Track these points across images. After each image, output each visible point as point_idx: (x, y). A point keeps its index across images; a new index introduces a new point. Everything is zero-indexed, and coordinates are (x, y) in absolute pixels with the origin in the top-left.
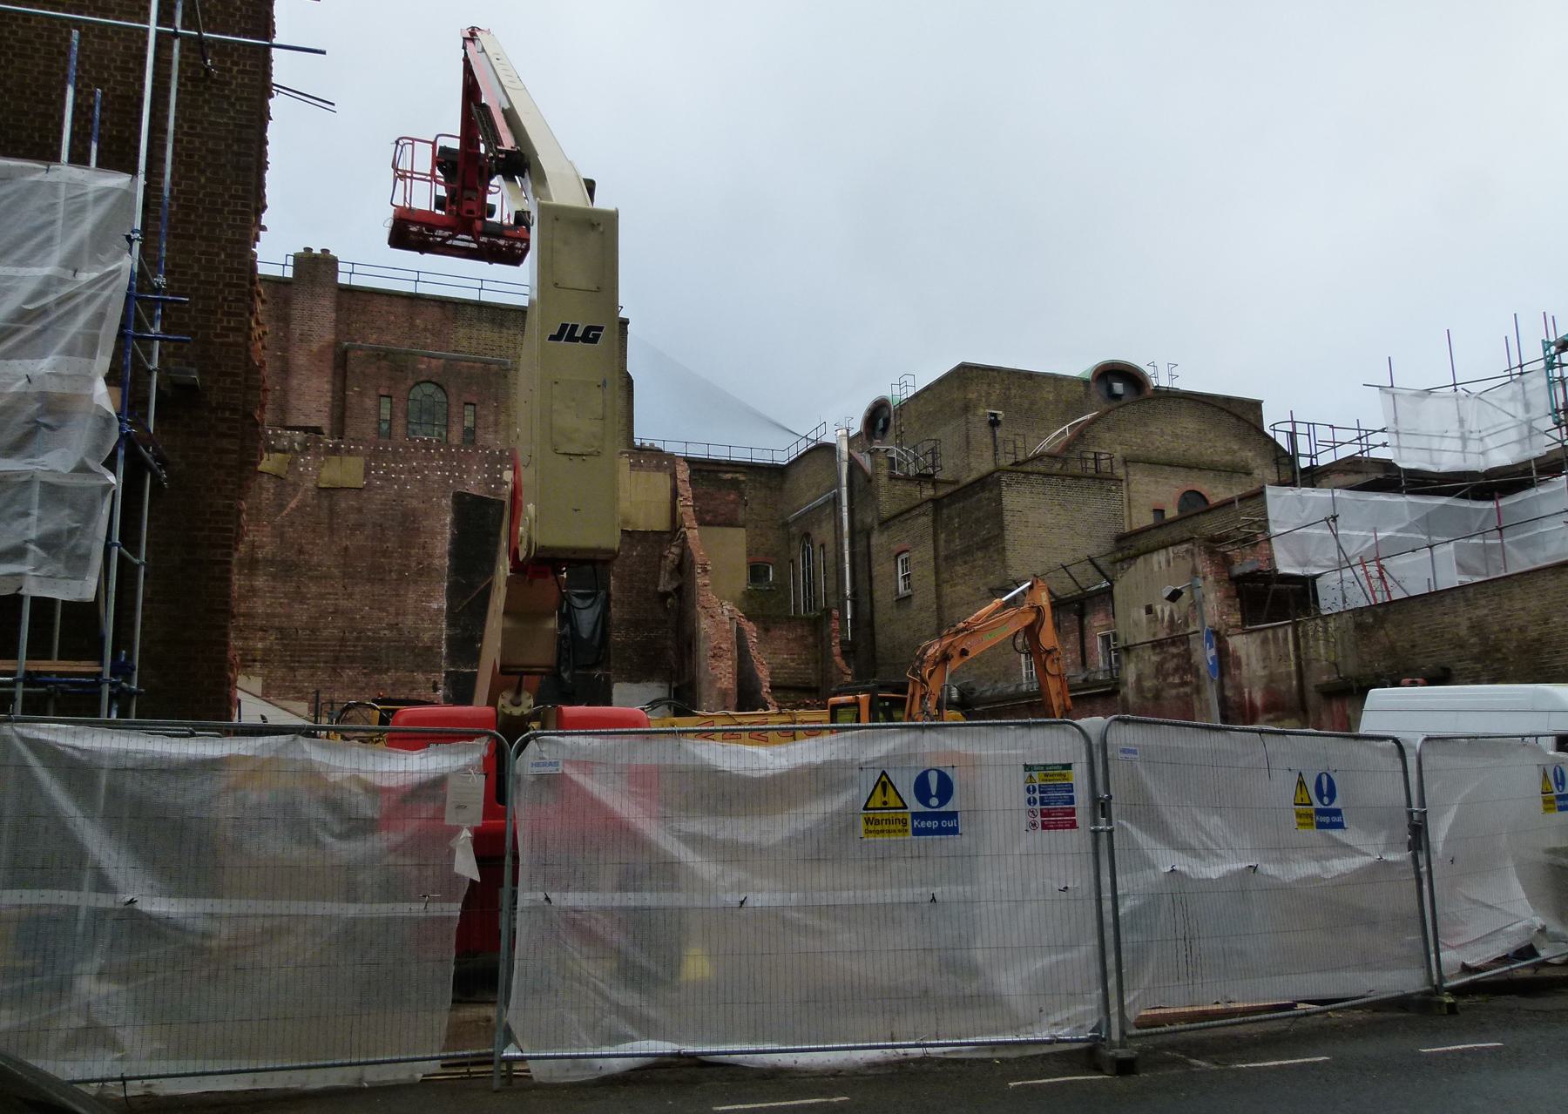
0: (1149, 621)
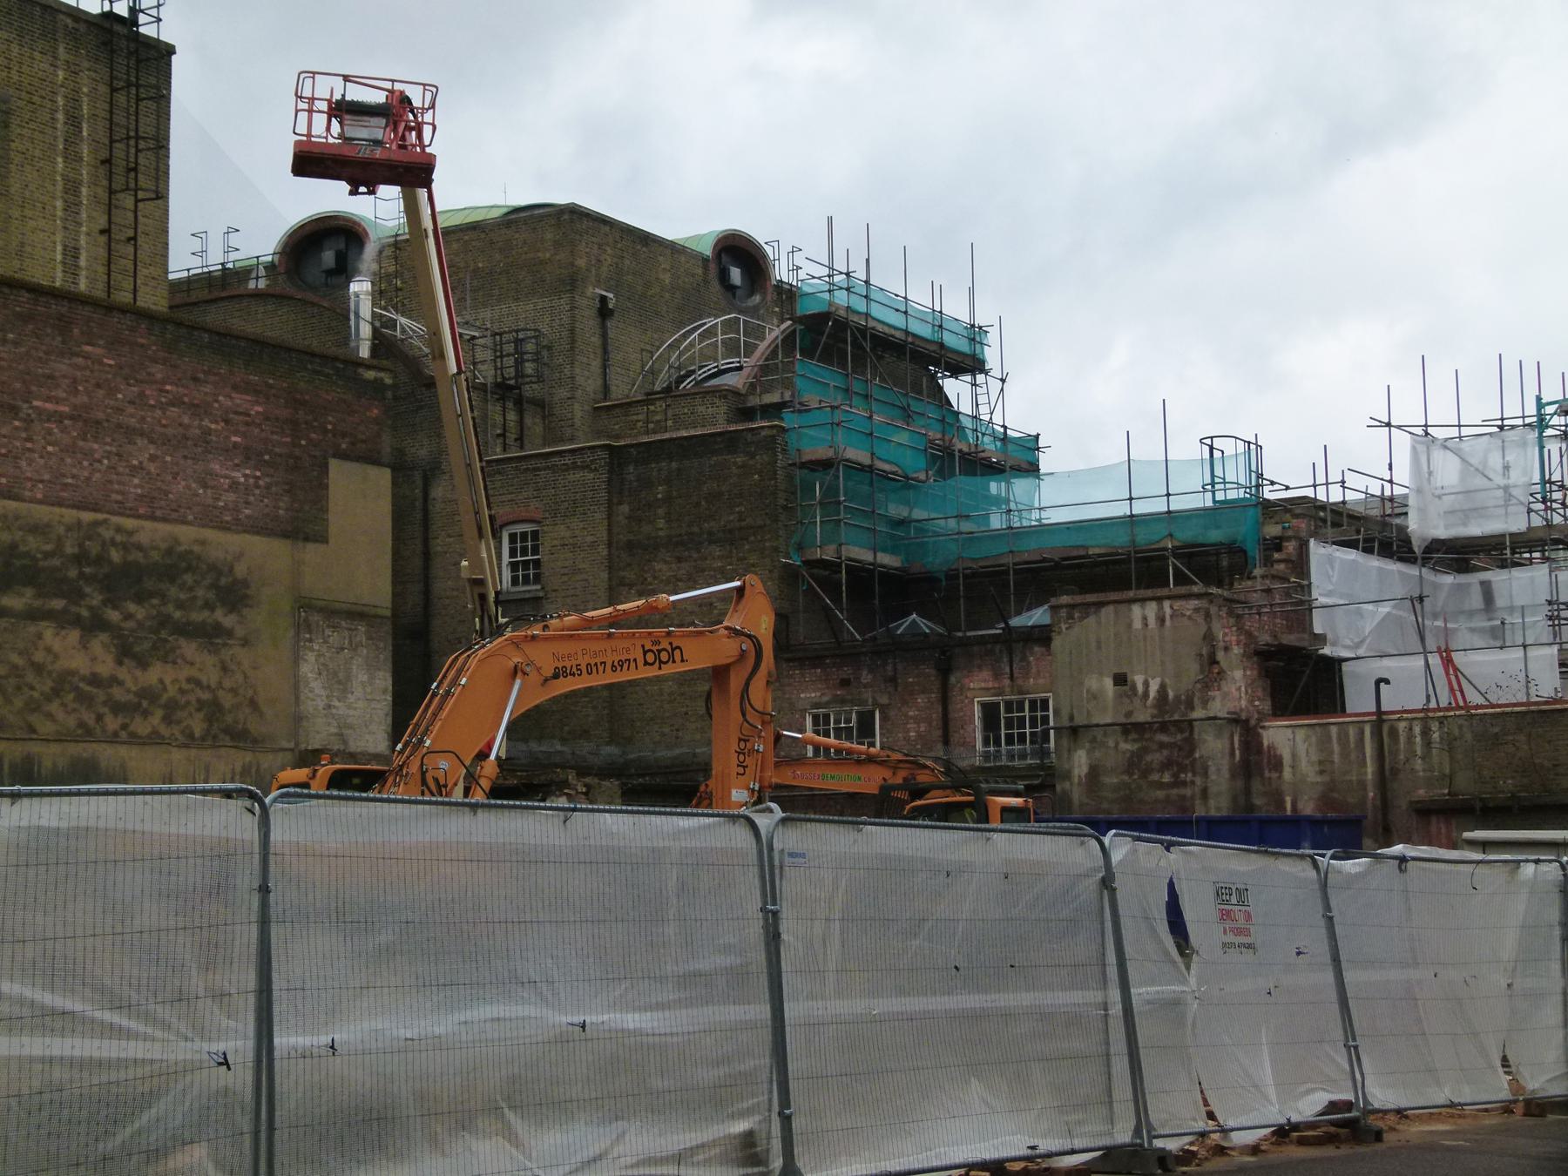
0: (1119, 697)
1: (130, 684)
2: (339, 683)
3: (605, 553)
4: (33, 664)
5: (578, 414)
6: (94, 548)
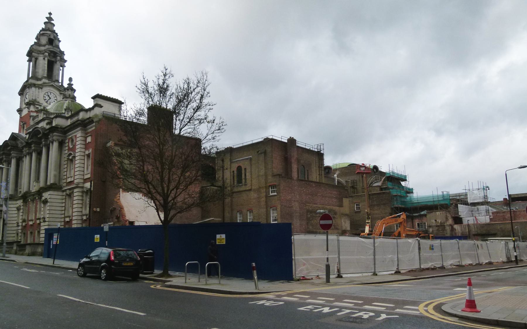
2: (345, 222)
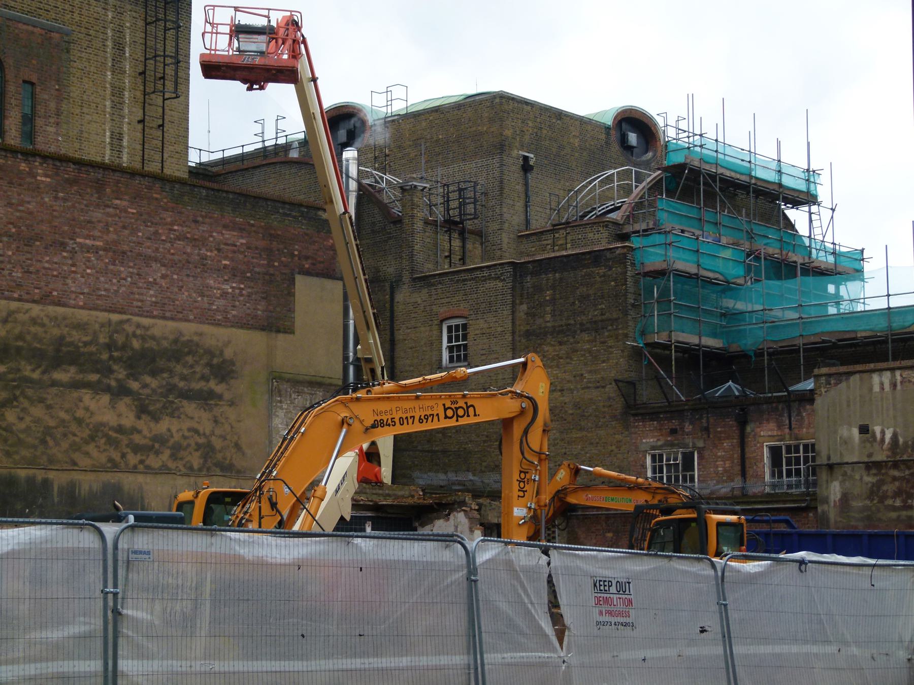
0: (863, 442)
1: (146, 432)
3: (510, 339)
4: (75, 419)
5: (505, 240)
6: (120, 339)
